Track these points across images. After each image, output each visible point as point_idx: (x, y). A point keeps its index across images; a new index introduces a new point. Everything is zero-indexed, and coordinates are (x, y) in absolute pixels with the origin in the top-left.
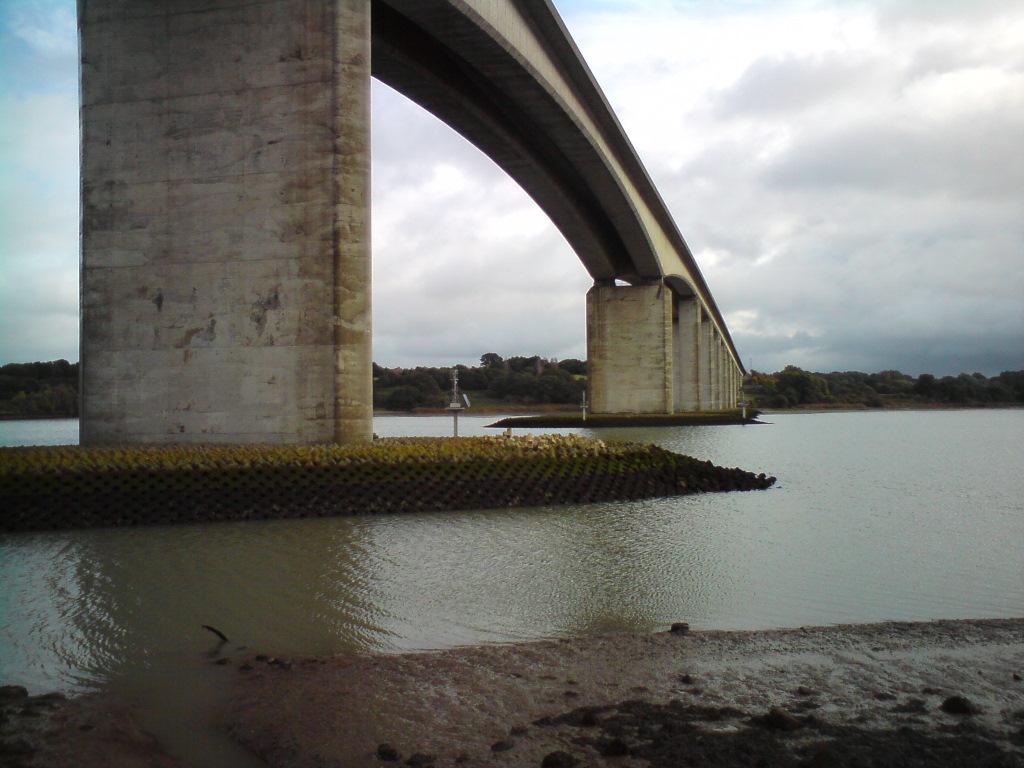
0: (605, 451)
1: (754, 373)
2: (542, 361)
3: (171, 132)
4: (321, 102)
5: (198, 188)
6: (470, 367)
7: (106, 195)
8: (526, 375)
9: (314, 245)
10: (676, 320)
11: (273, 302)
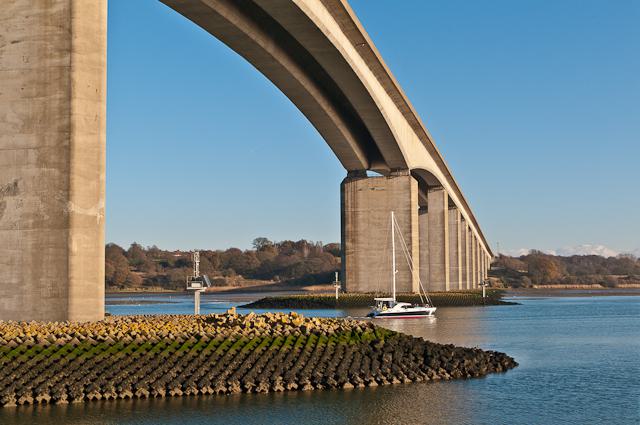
0: (318, 328)
1: (501, 256)
2: (308, 244)
6: (225, 250)
8: (296, 258)
9: (52, 138)
10: (423, 209)
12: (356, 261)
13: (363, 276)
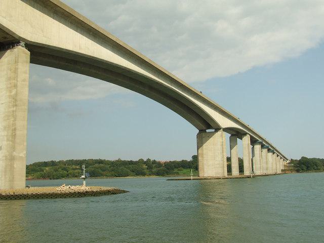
4: (14, 92)
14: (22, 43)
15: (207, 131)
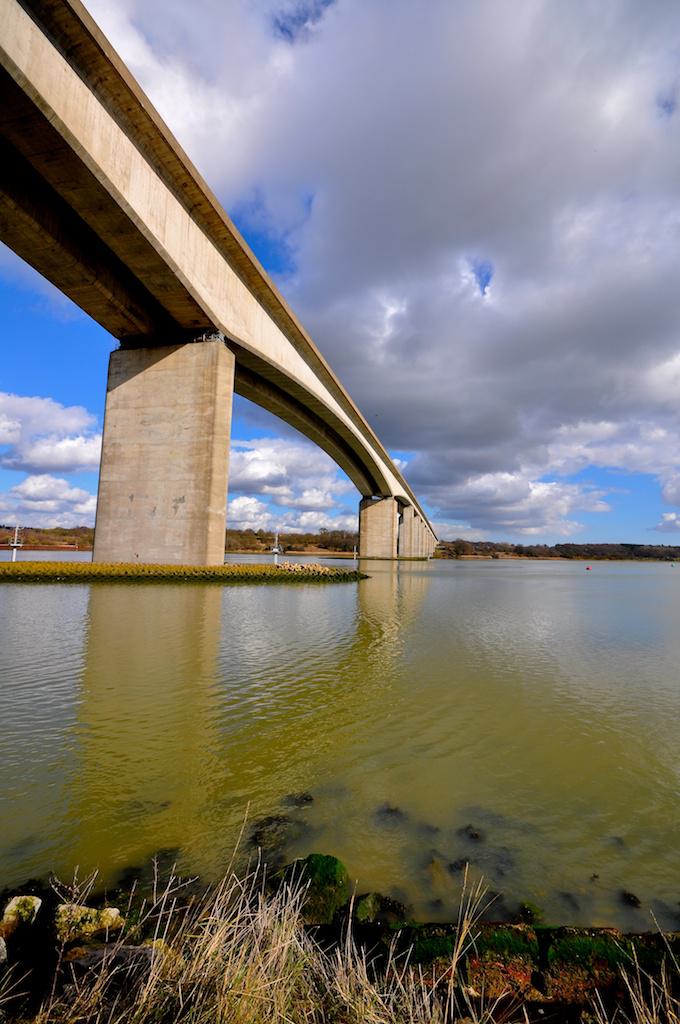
3: (143, 422)
4: (208, 412)
5: (152, 448)
7: (112, 449)
9: (202, 476)
11: (182, 500)
12: (366, 540)
13: (369, 548)
14: (222, 336)
15: (373, 497)
